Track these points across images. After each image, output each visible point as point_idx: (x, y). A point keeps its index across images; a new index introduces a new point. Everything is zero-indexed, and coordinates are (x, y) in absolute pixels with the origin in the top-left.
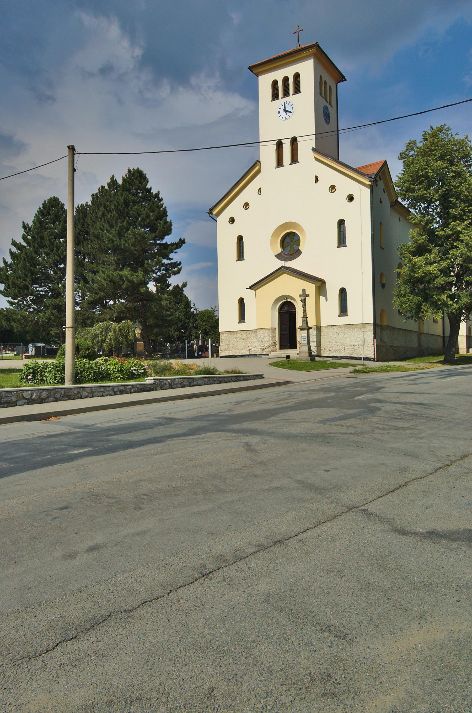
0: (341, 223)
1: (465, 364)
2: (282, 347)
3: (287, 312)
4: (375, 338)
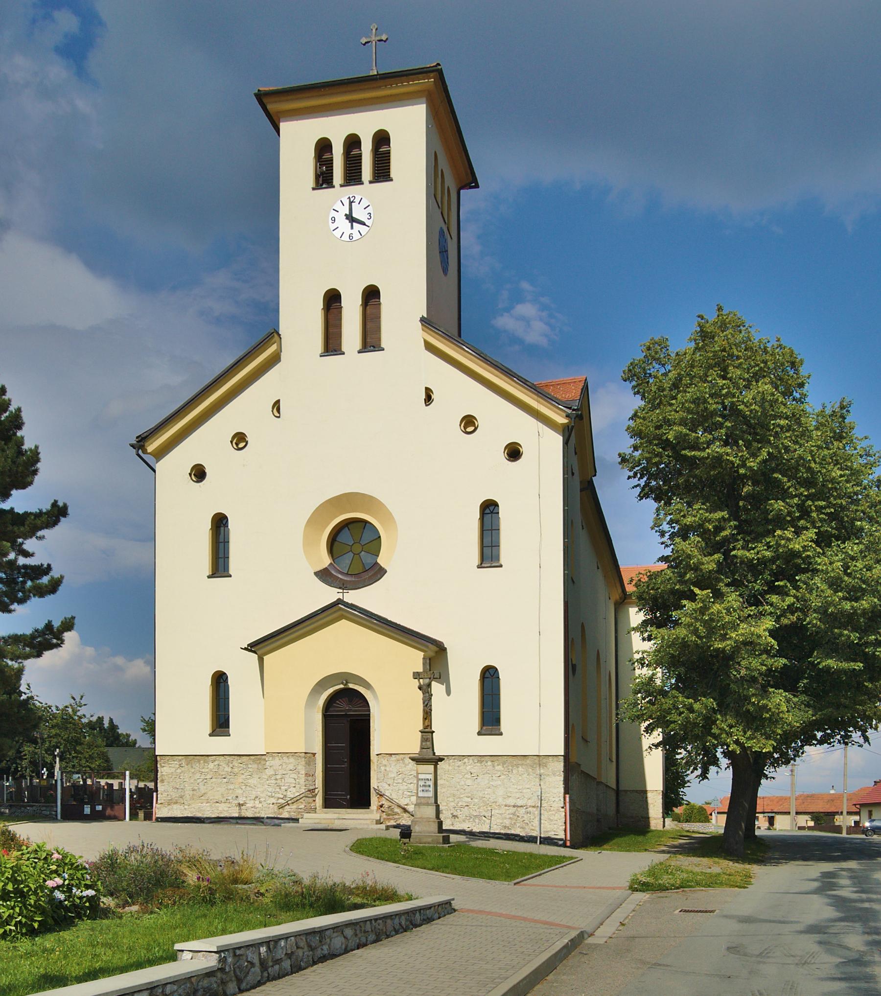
0: (489, 508)
2: (329, 803)
3: (346, 720)
4: (566, 792)
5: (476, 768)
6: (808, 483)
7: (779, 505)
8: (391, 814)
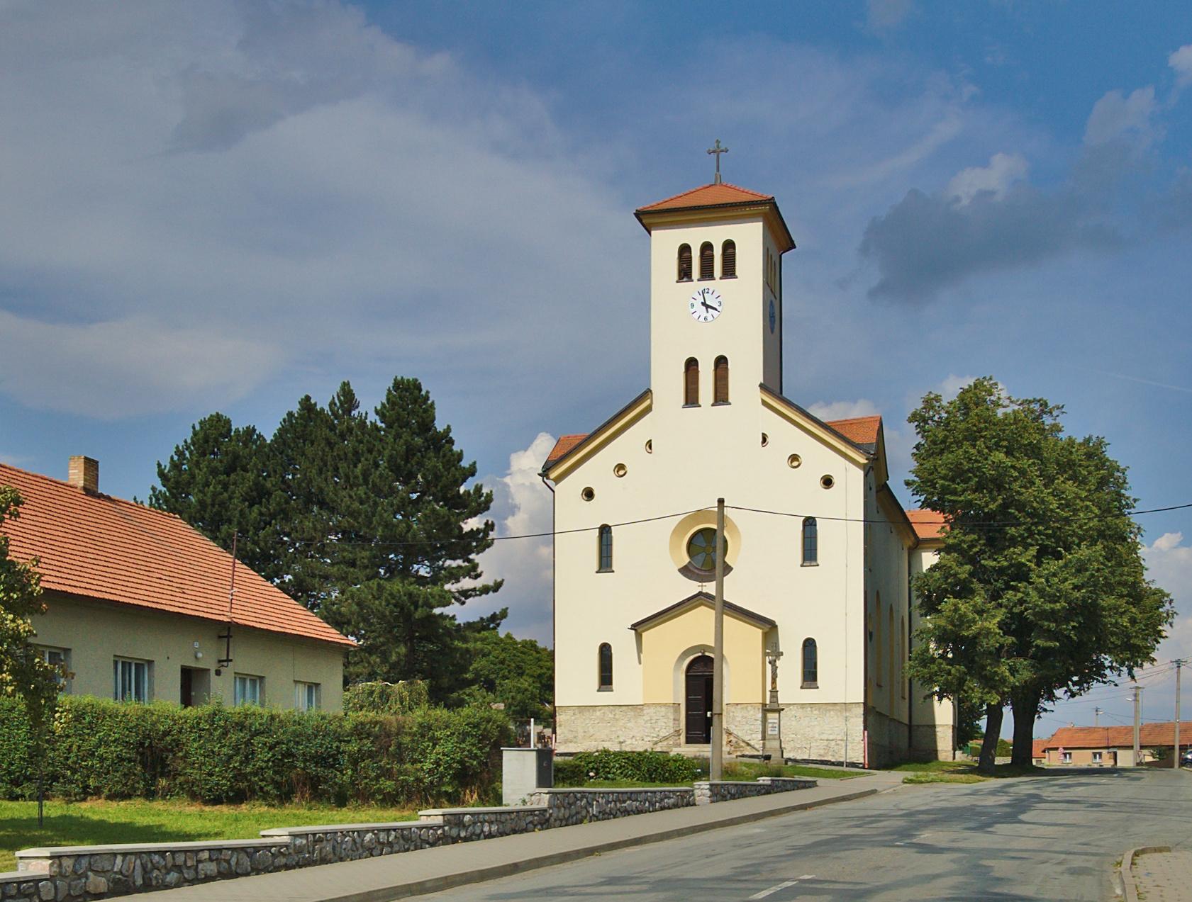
0: (809, 523)
1: (1020, 775)
2: (689, 741)
3: (701, 677)
5: (800, 713)
6: (1031, 515)
8: (737, 747)
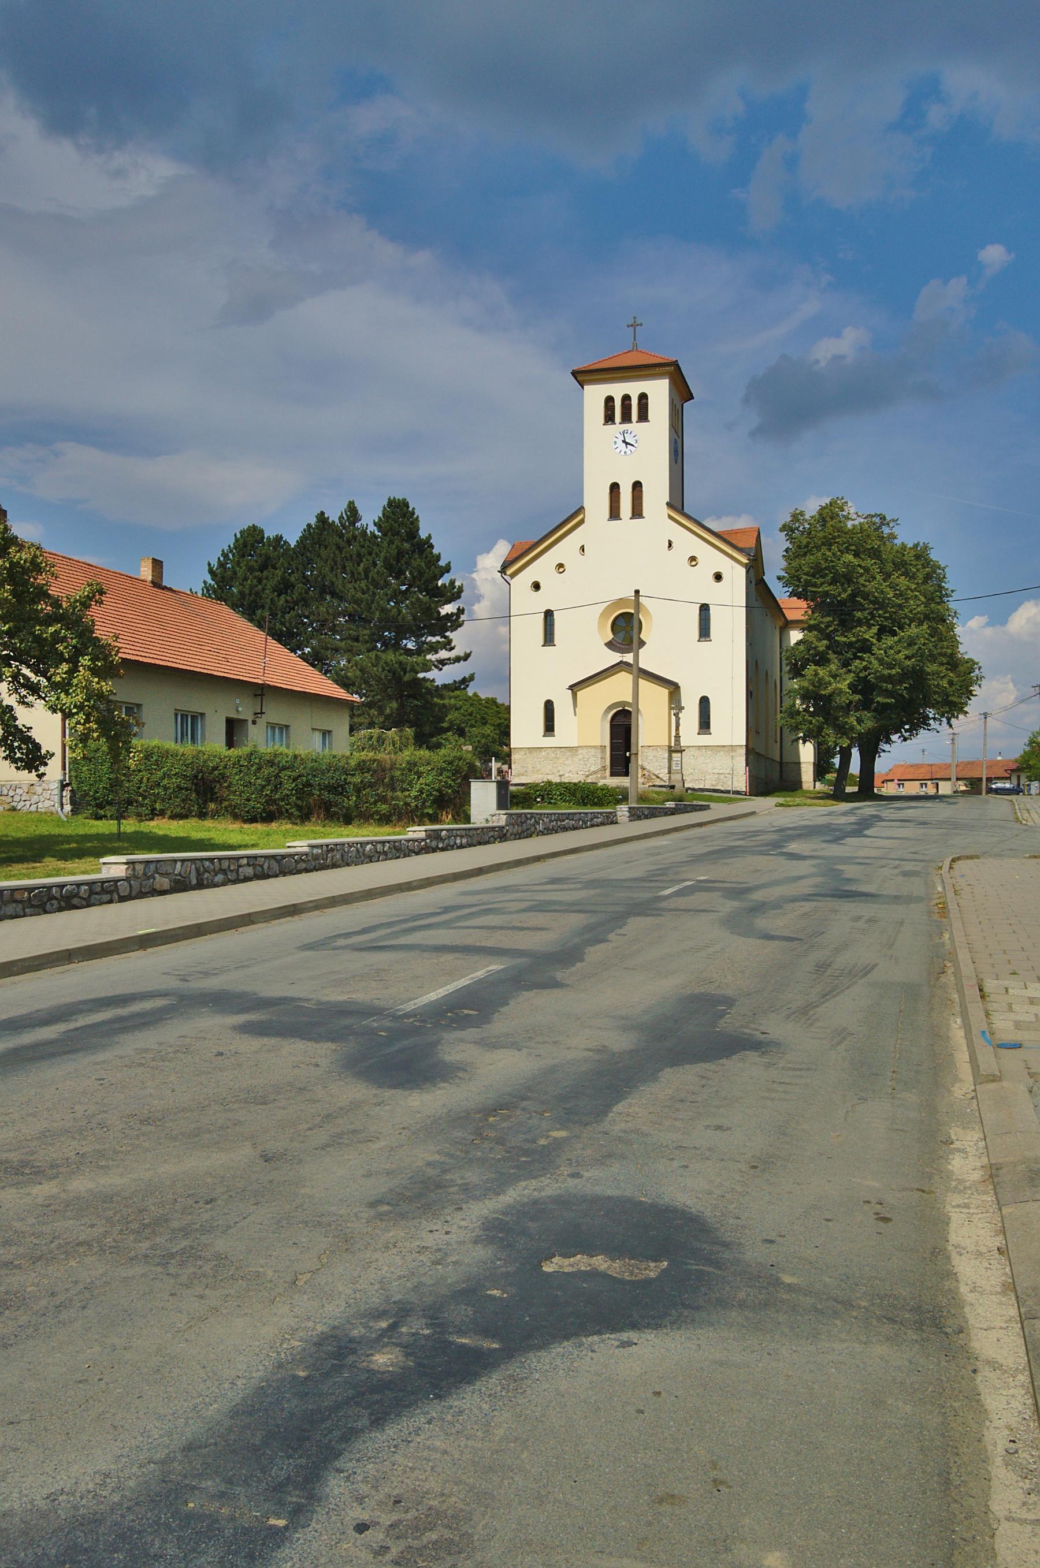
0: (704, 608)
1: (864, 801)
2: (613, 774)
3: (622, 726)
5: (697, 753)
7: (859, 614)
8: (649, 779)
